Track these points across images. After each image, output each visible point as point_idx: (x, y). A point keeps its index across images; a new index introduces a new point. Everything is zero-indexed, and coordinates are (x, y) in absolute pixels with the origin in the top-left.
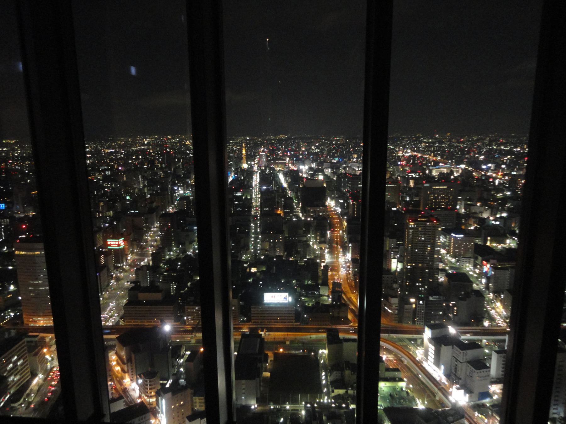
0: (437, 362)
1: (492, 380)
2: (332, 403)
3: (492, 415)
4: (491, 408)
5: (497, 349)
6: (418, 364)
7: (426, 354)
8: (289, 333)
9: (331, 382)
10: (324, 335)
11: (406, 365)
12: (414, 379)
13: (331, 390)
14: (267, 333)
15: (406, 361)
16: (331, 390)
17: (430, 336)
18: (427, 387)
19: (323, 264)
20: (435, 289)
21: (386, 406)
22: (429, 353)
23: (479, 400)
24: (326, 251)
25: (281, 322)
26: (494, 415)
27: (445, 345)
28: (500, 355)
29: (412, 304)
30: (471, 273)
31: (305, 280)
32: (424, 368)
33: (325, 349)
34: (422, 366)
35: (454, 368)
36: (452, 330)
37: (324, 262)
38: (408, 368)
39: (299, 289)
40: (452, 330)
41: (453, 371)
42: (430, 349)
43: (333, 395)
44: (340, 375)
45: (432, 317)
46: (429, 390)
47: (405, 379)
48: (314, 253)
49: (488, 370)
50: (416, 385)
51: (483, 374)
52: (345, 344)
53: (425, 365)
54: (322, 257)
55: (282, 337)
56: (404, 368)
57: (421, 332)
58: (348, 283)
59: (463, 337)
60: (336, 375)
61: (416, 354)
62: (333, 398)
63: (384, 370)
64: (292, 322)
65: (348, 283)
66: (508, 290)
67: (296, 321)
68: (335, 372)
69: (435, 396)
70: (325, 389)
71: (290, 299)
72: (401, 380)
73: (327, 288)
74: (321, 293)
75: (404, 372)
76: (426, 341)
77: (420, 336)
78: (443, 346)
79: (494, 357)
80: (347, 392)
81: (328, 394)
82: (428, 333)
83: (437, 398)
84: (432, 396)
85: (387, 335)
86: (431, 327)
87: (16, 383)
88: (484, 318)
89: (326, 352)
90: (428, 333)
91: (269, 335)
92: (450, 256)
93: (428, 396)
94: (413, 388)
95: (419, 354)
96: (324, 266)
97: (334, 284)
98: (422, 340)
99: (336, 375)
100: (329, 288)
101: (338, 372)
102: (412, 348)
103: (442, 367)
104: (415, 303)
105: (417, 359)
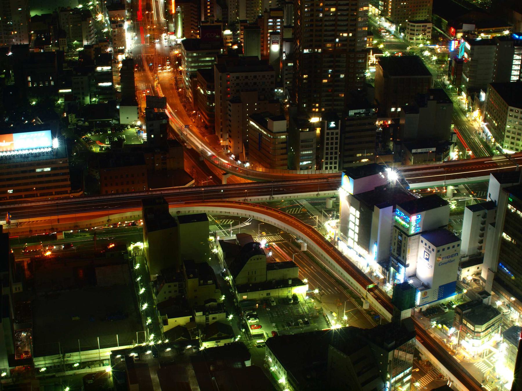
0: (365, 240)
1: (463, 260)
2: (164, 346)
3: (461, 323)
4: (459, 310)
5: (473, 203)
6: (330, 247)
7: (345, 230)
8: (60, 217)
9: (158, 305)
10: (138, 213)
11: (304, 252)
12: (323, 279)
13: (160, 321)
14: (12, 222)
15: (305, 243)
16: (160, 321)
17: (352, 192)
18: (346, 288)
19: (121, 57)
20: (360, 93)
21: (271, 335)
22: (351, 225)
23: (439, 299)
24: (127, 25)
25: (41, 195)
26: (464, 322)
27: (380, 207)
28: (477, 213)
29: (312, 127)
30: (427, 53)
31: (84, 95)
32: (340, 254)
33: (142, 241)
34: (336, 250)
35: (396, 247)
36: (392, 175)
37: (122, 52)
38: (309, 258)
39: (72, 119)
40: (392, 175)
41: (395, 253)
42: (351, 218)
43: (165, 329)
44: (177, 288)
45: (354, 150)
46: (290, 186)
47: (305, 281)
48: (99, 32)
49: (455, 244)
50: (326, 287)
51: (447, 253)
52: (184, 228)
53: (342, 247)
54: (117, 39)
55: (48, 226)
56: (302, 259)
57: (336, 185)
58: (180, 94)
59: (412, 186)
60: (168, 290)
61: (324, 229)
62: (167, 334)
63: (265, 266)
64: (66, 192)
65: (180, 94)
66: (493, 85)
67: (75, 188)
68: (166, 285)
69: (361, 304)
70: (149, 321)
71: (56, 143)
72: (298, 282)
73: (136, 107)
74: (123, 120)
75: (303, 267)
76: (344, 203)
77: (331, 193)
78: (376, 208)
79: (468, 217)
80: (193, 320)
81: (155, 328)
82: (347, 186)
83: (366, 307)
84: (356, 304)
85: (268, 197)
86: (353, 174)
87: (34, 177)
88: (451, 144)
89: (143, 245)
90: (347, 186)
91: (17, 225)
92: (387, 20)
93: (350, 305)
94: (321, 295)
95: (330, 228)
96: (124, 62)
97: (149, 99)
98: (337, 198)
99: (168, 290)
100: (140, 109)
101: (172, 284)
102: (318, 218)
103: (375, 248)
104: (321, 124)
105: (327, 238)
